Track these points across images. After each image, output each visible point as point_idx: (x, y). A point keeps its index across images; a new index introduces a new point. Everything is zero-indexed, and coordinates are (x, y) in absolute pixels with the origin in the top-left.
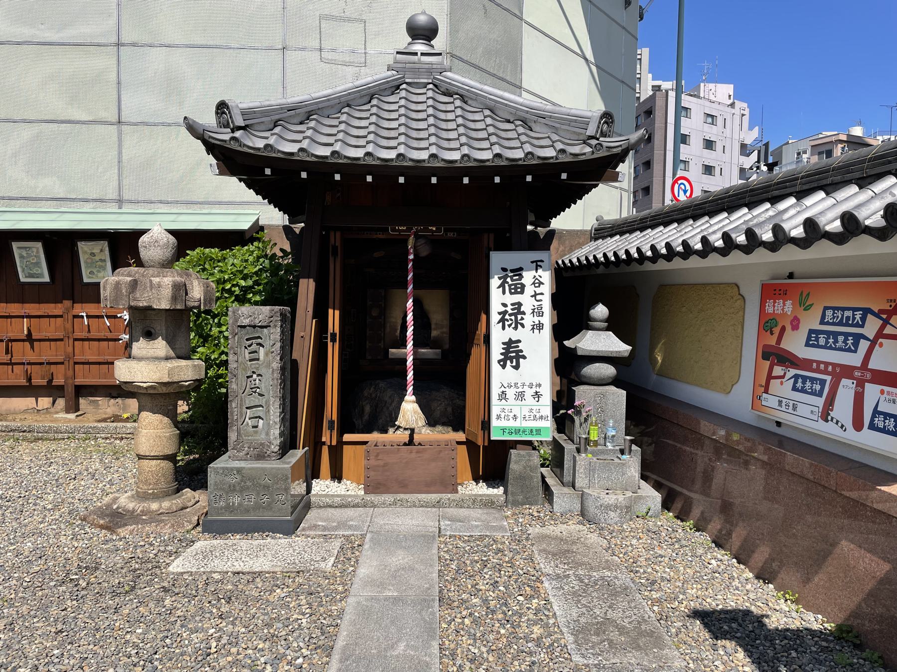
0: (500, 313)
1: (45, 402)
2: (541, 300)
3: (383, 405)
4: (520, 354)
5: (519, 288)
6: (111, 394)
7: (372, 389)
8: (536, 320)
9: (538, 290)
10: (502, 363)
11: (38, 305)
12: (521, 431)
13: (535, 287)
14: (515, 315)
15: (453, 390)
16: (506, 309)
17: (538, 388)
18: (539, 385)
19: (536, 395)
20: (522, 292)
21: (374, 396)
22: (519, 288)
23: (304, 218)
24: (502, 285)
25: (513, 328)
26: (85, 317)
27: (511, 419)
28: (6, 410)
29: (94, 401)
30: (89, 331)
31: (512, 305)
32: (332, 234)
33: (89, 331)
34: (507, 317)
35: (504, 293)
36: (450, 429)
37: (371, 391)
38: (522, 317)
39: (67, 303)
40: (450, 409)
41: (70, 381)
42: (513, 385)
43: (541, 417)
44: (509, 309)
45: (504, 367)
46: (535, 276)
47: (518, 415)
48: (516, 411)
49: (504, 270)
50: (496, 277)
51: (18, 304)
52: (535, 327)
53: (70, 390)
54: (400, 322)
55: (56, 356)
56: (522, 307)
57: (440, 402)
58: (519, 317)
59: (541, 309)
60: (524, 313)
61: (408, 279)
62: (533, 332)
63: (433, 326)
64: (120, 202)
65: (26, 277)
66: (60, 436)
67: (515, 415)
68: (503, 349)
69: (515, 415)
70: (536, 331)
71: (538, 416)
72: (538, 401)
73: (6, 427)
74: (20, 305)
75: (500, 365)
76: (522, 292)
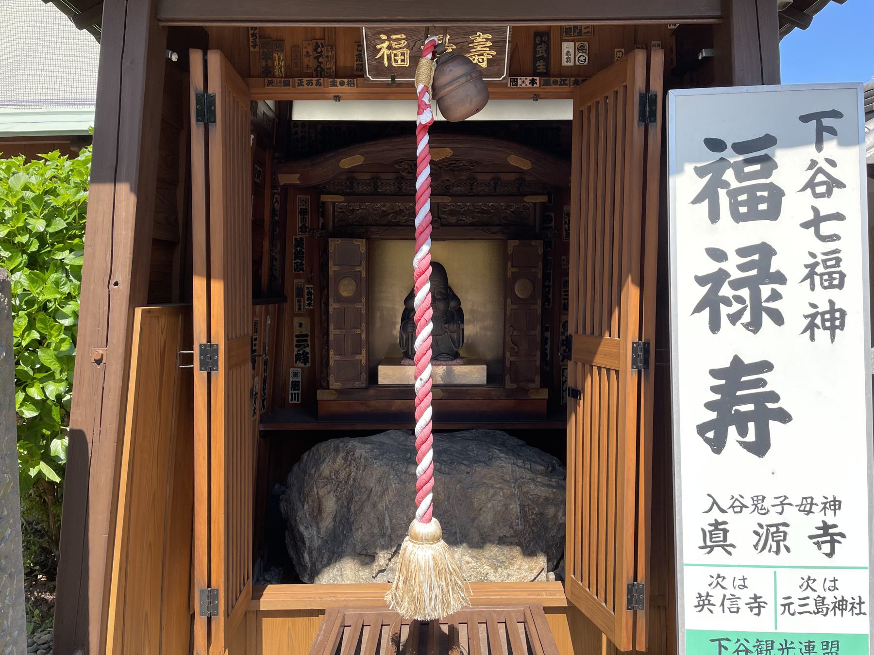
0: (701, 281)
2: (835, 237)
3: (365, 497)
4: (770, 406)
5: (762, 200)
7: (339, 461)
8: (822, 298)
9: (826, 207)
10: (710, 435)
12: (777, 646)
13: (816, 196)
14: (753, 284)
15: (520, 463)
16: (724, 265)
17: (830, 513)
18: (835, 505)
19: (826, 534)
20: (773, 213)
21: (343, 475)
22: (762, 200)
24: (708, 195)
25: (747, 326)
27: (744, 609)
31: (741, 252)
32: (196, 57)
34: (726, 291)
35: (714, 216)
36: (516, 551)
37: (336, 466)
38: (773, 290)
40: (515, 507)
42: (748, 501)
43: (841, 605)
44: (732, 266)
45: (718, 445)
46: (814, 163)
47: (767, 596)
48: (759, 584)
49: (715, 145)
50: (689, 168)
52: (818, 321)
54: (401, 308)
56: (774, 259)
57: (492, 491)
58: (766, 290)
59: (837, 265)
60: (780, 279)
61: (418, 185)
62: (812, 338)
63: (466, 317)
67: (756, 598)
68: (714, 389)
69: (756, 598)
70: (822, 335)
71: (829, 600)
72: (830, 555)
75: (707, 440)
76: (773, 213)
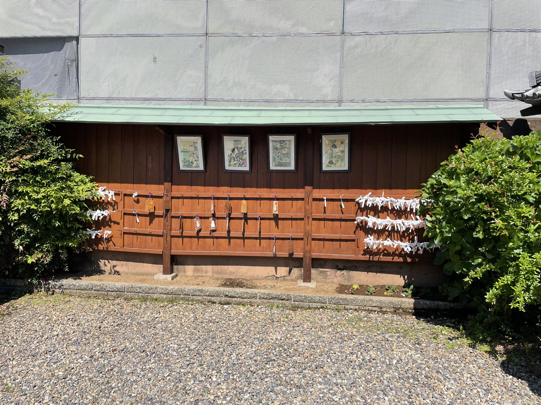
1: (283, 271)
6: (337, 266)
11: (120, 184)
23: (222, 135)
26: (325, 200)
28: (250, 276)
29: (323, 272)
30: (325, 212)
33: (325, 212)
39: (308, 188)
41: (308, 255)
51: (266, 189)
53: (308, 262)
55: (297, 232)
64: (340, 102)
65: (276, 166)
66: (314, 305)
73: (268, 295)
74: (268, 189)
